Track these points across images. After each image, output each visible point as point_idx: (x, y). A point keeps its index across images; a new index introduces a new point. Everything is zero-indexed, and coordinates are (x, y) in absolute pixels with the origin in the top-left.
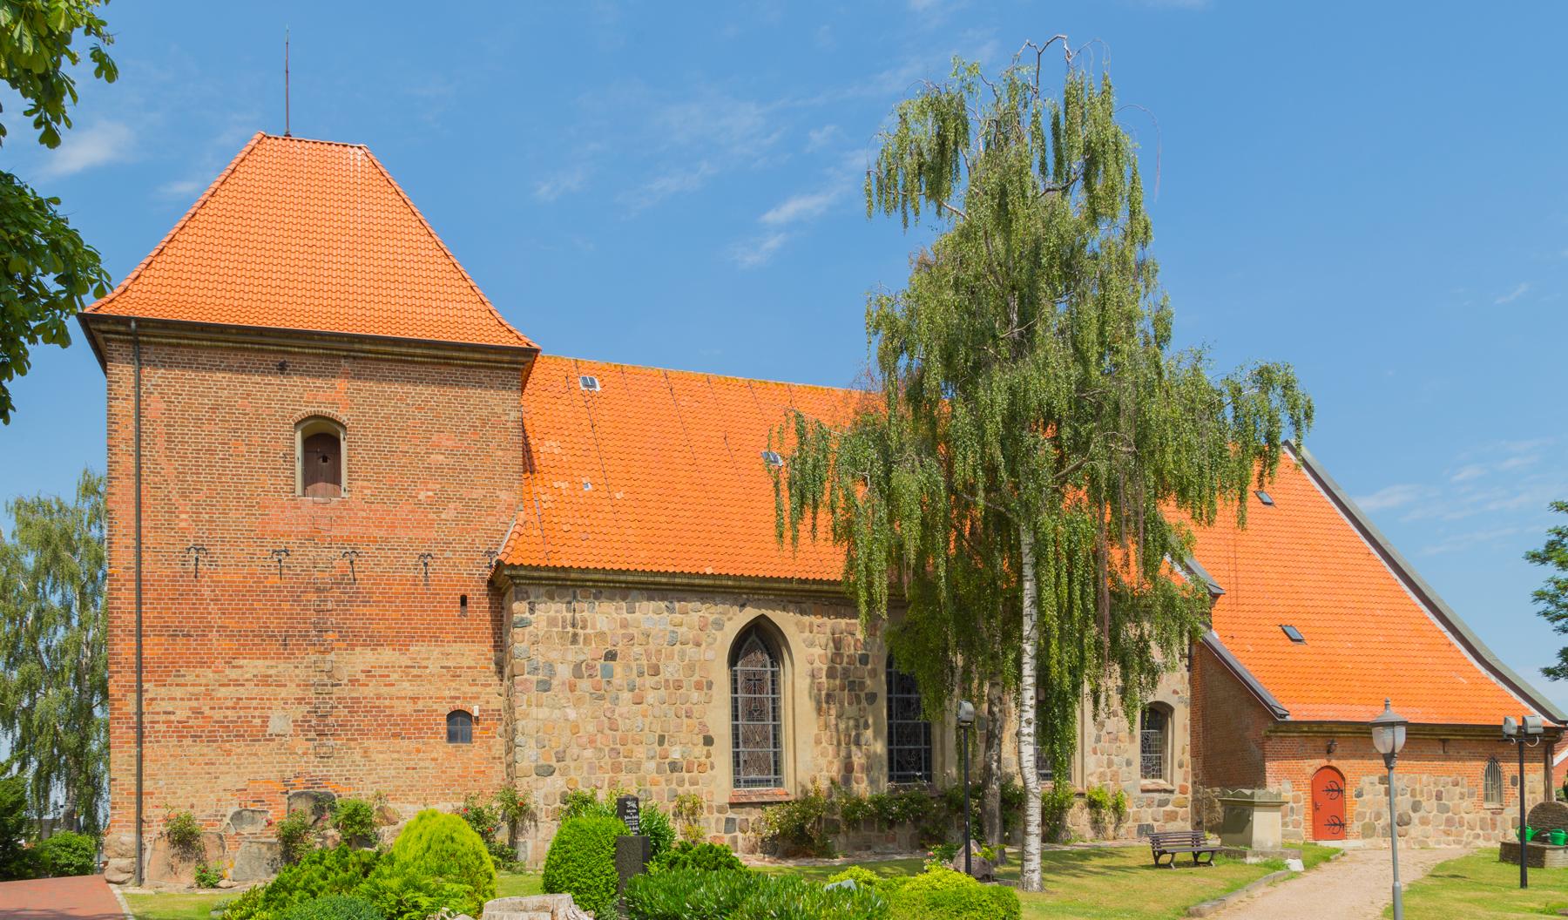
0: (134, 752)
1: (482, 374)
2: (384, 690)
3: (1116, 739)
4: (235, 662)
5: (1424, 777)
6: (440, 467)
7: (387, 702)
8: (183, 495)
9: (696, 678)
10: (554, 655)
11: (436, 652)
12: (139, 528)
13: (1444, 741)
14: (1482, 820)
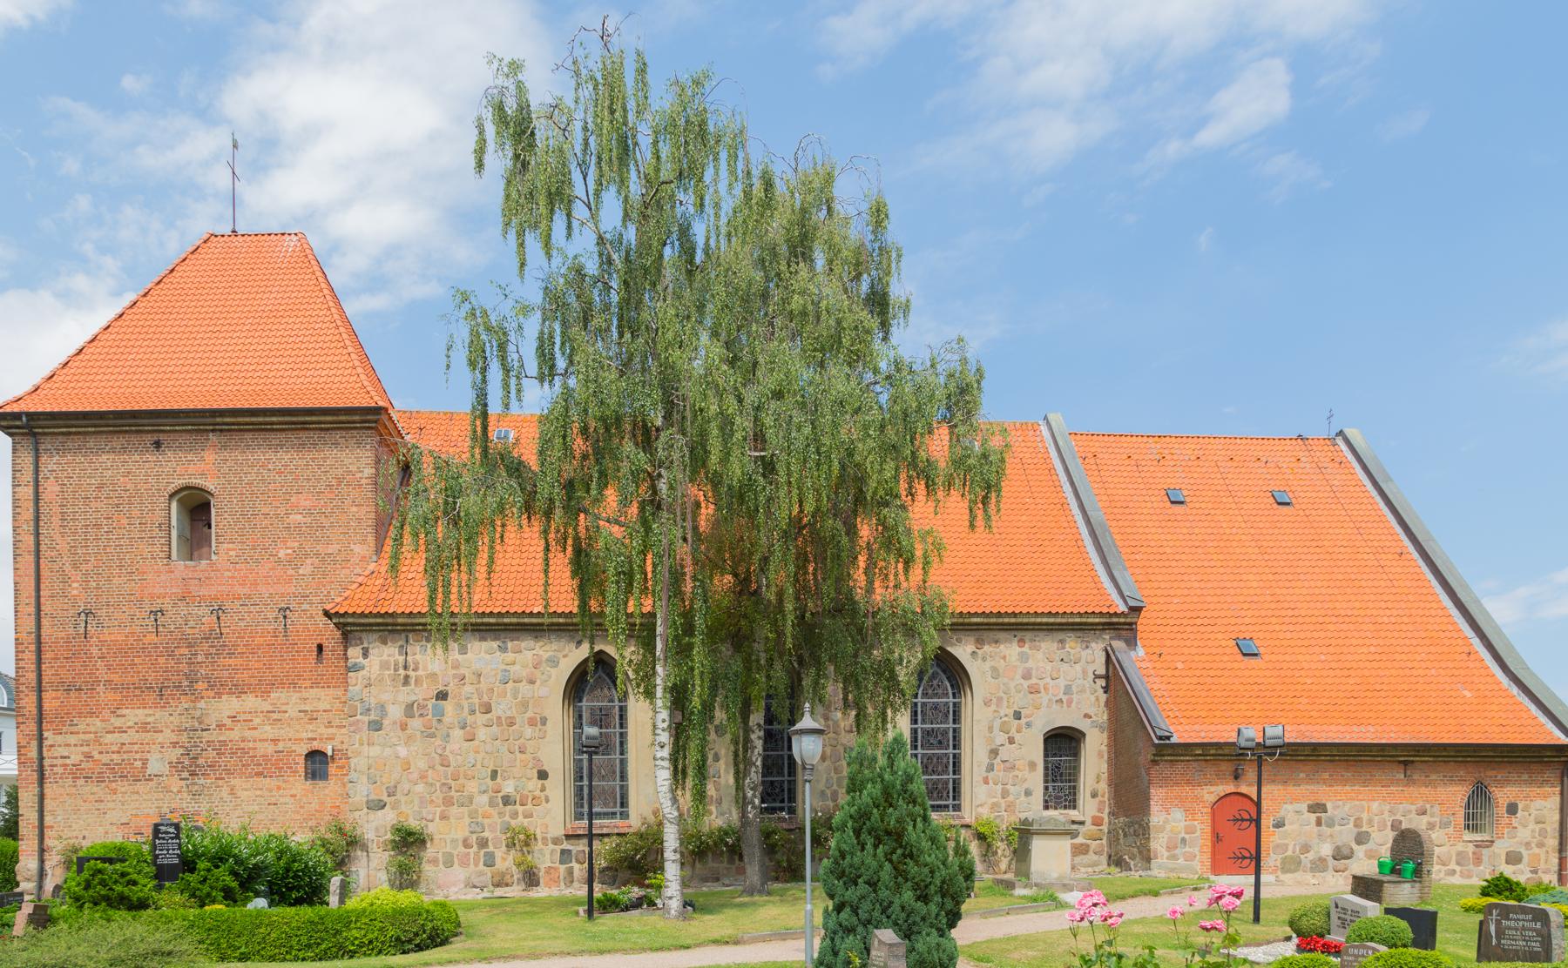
0: (36, 791)
1: (338, 435)
2: (248, 734)
3: (1013, 767)
4: (119, 712)
5: (1375, 805)
6: (299, 526)
7: (251, 745)
8: (75, 567)
9: (529, 714)
10: (385, 697)
11: (295, 697)
12: (38, 597)
13: (1405, 763)
14: (1459, 854)
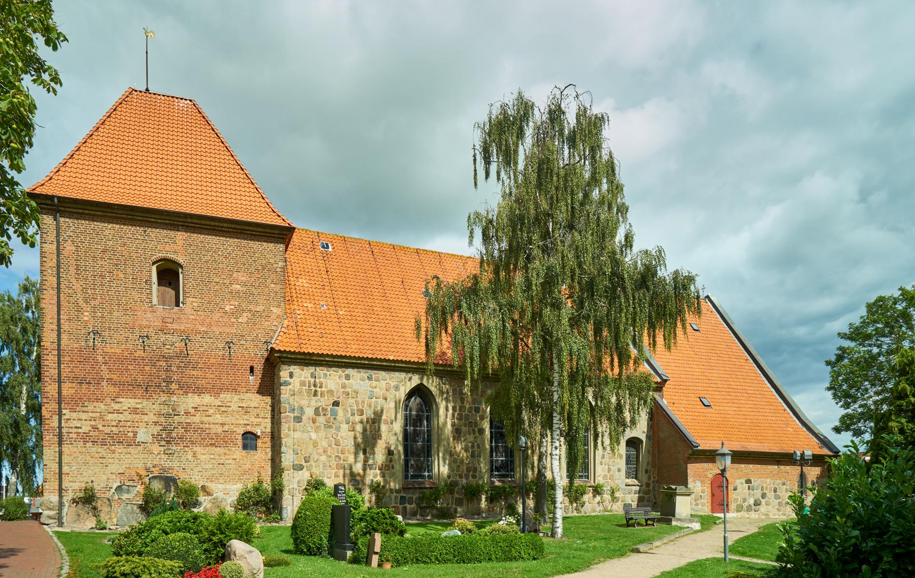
2: (206, 419)
4: (117, 400)
6: (238, 292)
7: (207, 426)
10: (304, 402)
11: (236, 398)
12: (59, 320)
